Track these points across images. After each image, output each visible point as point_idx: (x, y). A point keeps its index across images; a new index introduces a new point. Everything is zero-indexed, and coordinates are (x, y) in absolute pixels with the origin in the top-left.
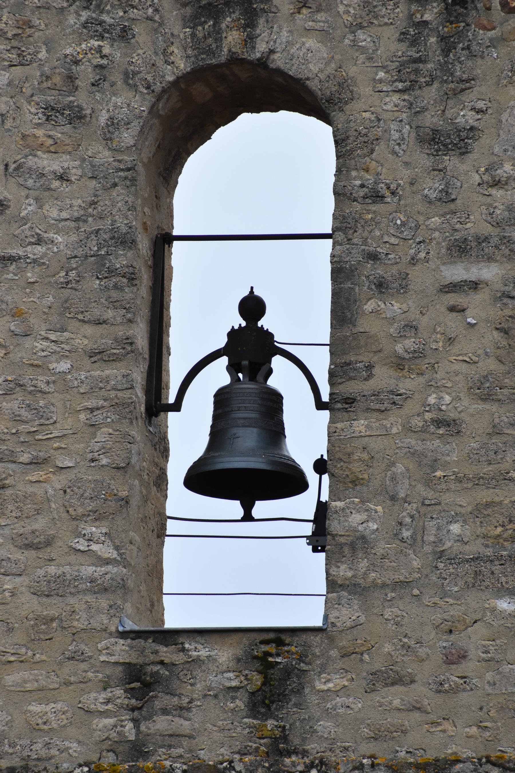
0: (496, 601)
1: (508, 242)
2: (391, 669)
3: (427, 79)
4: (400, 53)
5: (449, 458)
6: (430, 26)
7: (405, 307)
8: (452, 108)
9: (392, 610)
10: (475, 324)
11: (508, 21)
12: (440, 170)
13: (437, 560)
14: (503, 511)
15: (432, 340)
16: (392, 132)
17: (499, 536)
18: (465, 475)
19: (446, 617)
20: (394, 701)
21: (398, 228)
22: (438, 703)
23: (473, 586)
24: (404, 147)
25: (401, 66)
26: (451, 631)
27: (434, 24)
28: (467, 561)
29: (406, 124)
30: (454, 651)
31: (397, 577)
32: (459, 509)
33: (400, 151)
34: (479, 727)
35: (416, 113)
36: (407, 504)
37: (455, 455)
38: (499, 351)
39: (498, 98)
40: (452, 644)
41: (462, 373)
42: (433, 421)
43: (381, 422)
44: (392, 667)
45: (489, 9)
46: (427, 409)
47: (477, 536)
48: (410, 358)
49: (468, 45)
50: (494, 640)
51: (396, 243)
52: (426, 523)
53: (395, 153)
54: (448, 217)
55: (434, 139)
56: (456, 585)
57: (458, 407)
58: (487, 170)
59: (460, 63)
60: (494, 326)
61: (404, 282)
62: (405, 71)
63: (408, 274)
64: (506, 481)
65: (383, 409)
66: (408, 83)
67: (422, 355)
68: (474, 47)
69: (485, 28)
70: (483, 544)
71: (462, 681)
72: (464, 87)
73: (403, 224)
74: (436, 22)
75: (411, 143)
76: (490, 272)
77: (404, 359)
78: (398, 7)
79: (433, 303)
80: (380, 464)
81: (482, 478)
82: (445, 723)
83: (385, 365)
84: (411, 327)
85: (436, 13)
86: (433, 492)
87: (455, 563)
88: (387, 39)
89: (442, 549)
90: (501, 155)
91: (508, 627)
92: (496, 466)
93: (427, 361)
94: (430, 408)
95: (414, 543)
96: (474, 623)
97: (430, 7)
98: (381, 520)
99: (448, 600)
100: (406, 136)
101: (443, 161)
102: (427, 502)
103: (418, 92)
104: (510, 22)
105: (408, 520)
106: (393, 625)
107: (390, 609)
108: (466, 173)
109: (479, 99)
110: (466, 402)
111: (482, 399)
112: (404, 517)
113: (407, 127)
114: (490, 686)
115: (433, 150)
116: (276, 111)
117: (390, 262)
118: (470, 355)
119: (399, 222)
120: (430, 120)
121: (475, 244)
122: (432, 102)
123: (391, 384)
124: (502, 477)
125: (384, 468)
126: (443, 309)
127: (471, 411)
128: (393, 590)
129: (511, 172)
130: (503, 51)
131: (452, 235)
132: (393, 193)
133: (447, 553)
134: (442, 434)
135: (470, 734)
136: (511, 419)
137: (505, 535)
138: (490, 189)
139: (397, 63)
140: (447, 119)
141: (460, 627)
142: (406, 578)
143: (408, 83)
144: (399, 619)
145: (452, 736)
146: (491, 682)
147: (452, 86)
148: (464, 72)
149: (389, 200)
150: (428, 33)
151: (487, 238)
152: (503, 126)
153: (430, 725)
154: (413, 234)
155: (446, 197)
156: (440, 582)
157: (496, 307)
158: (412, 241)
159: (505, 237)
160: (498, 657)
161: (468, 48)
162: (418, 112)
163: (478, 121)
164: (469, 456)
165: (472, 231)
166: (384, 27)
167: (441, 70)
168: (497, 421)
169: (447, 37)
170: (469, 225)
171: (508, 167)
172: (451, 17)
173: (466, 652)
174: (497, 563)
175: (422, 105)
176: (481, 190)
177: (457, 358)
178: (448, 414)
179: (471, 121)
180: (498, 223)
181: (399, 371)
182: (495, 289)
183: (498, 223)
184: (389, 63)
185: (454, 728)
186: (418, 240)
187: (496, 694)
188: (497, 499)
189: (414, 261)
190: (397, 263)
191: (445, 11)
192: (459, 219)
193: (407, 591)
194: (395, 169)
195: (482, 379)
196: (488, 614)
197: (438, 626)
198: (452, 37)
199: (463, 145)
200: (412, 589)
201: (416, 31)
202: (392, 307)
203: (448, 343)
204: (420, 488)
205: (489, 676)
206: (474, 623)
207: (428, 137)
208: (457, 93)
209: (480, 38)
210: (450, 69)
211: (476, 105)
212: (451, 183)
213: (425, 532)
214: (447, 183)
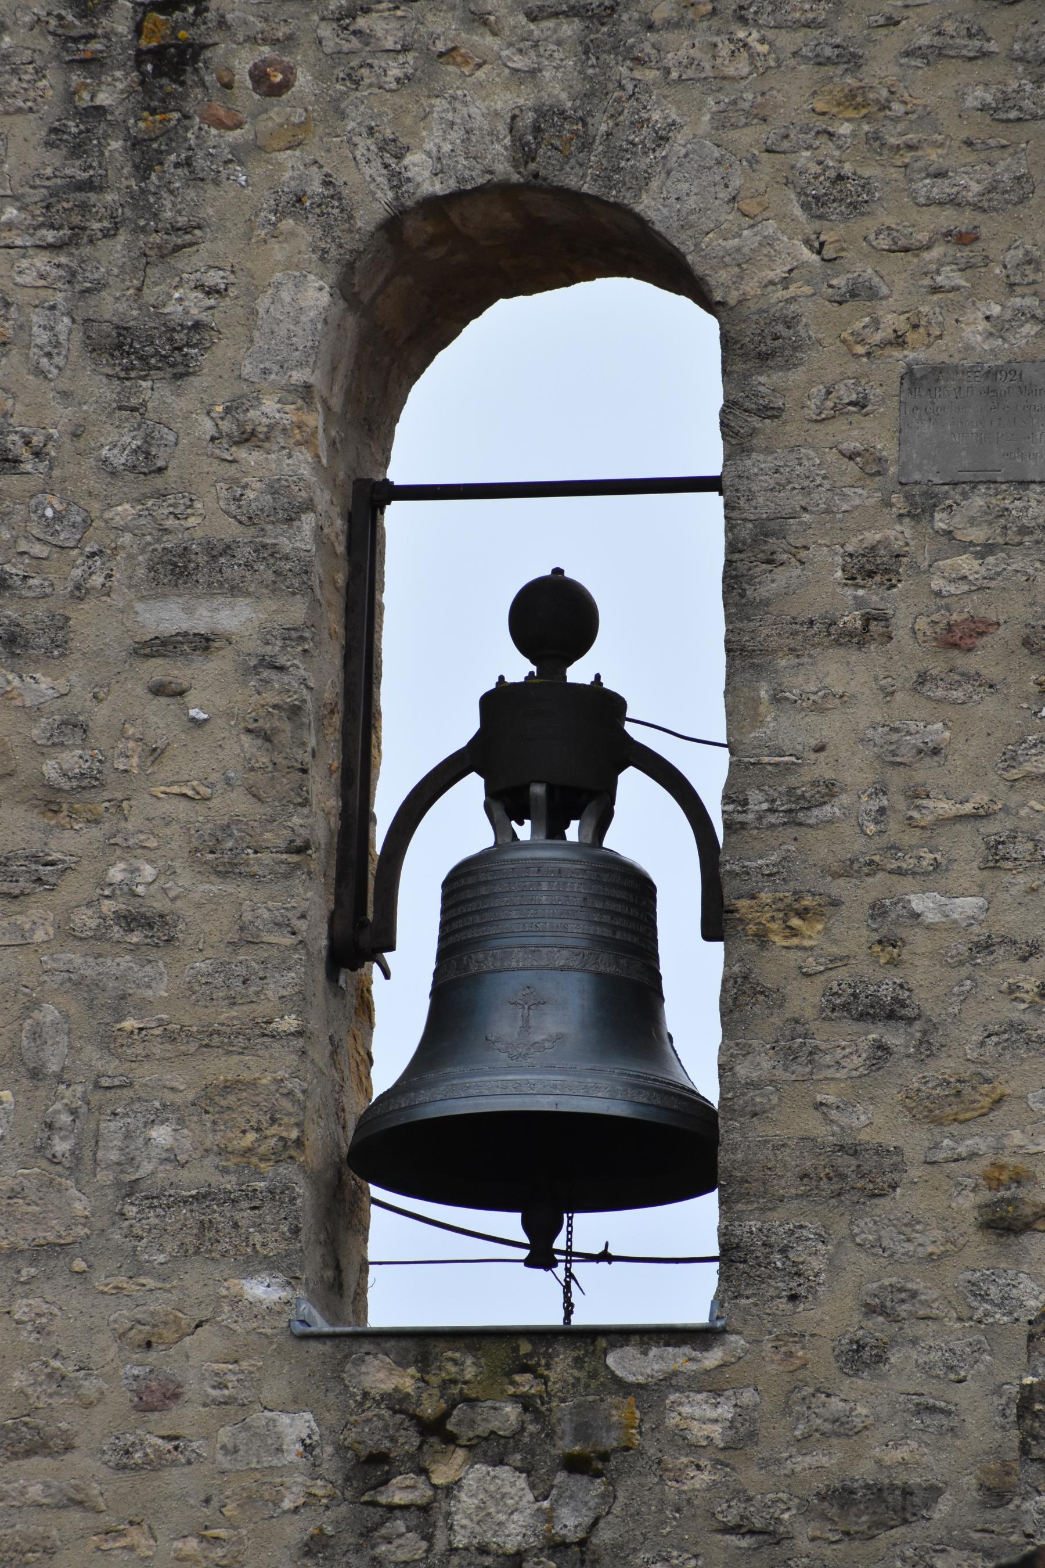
1: (272, 555)
2: (26, 1424)
3: (106, 224)
4: (49, 171)
5: (150, 992)
6: (109, 118)
7: (62, 686)
8: (156, 284)
10: (205, 720)
11: (266, 111)
12: (133, 409)
13: (123, 1199)
14: (258, 1099)
15: (117, 752)
16: (35, 329)
17: (250, 1150)
19: (139, 1316)
20: (31, 1489)
21: (48, 526)
23: (197, 1252)
24: (59, 360)
25: (51, 196)
28: (185, 1202)
29: (63, 314)
30: (154, 1385)
32: (169, 1097)
33: (52, 369)
34: (202, 1538)
35: (84, 291)
36: (63, 1087)
37: (163, 986)
38: (253, 777)
39: (249, 265)
40: (151, 1371)
41: (178, 821)
43: (12, 919)
44: (26, 1419)
45: (228, 86)
46: (106, 893)
47: (206, 1151)
48: (73, 789)
50: (236, 1362)
51: (44, 555)
52: (103, 1125)
53: (40, 372)
54: (150, 503)
55: (120, 346)
57: (170, 889)
58: (228, 410)
59: (171, 192)
60: (242, 725)
61: (61, 634)
62: (59, 207)
63: (68, 619)
64: (265, 1039)
65: (17, 892)
66: (67, 232)
67: (96, 783)
69: (220, 124)
70: (217, 1168)
71: (169, 1446)
72: (179, 241)
73: (59, 517)
74: (121, 109)
75: (74, 353)
76: (235, 617)
78: (44, 76)
79: (119, 678)
82: (133, 1531)
83: (22, 802)
84: (75, 726)
85: (122, 92)
86: (117, 1062)
89: (133, 1178)
91: (265, 1335)
92: (245, 1008)
94: (113, 891)
95: (77, 1165)
96: (197, 1326)
98: (11, 1119)
99: (143, 1281)
100: (62, 338)
102: (105, 1082)
103: (87, 251)
104: (272, 114)
105: (65, 1118)
106: (31, 1332)
107: (25, 1301)
108: (187, 416)
109: (210, 267)
110: (185, 878)
111: (218, 873)
112: (59, 1112)
113: (66, 320)
114: (226, 1455)
115: (118, 369)
116: (593, 279)
117: (31, 594)
118: (195, 783)
119: (49, 513)
120: (113, 306)
122: (116, 271)
123: (34, 842)
124: (258, 1032)
125: (16, 1014)
126: (140, 690)
127: (196, 897)
128: (33, 1262)
129: (277, 415)
131: (158, 541)
132: (37, 454)
133: (143, 1185)
134: (136, 944)
135: (183, 1554)
136: (277, 913)
137: (262, 1150)
138: (234, 449)
139: (44, 191)
140: (147, 305)
141: (169, 1335)
142: (60, 1237)
143: (67, 232)
144: (44, 1320)
145: (147, 1557)
146: (230, 1446)
147: (155, 238)
149: (28, 467)
150: (105, 131)
151: (228, 547)
152: (260, 322)
153: (102, 1536)
154: (78, 537)
155: (146, 464)
156: (129, 1244)
157: (247, 686)
158: (76, 551)
159: (264, 546)
160: (243, 1395)
161: (188, 163)
162: (88, 290)
164: (191, 989)
165: (199, 534)
167: (134, 206)
168: (248, 916)
169: (144, 140)
170: (192, 521)
171: (270, 405)
172: (151, 99)
173: (179, 1386)
174: (245, 1204)
175: (96, 276)
177: (168, 790)
178: (148, 902)
179: (194, 311)
180: (250, 518)
181: (50, 814)
182: (245, 650)
183: (250, 518)
184: (27, 189)
185: (152, 1542)
186: (88, 549)
187: (238, 1471)
188: (246, 1076)
189: (80, 592)
190: (46, 596)
191: (140, 88)
192: (171, 509)
193: (61, 1263)
195: (219, 833)
196: (226, 1309)
197: (124, 1334)
198: (155, 140)
199: (179, 359)
200: (72, 1260)
201: (82, 127)
202: (35, 686)
203: (151, 758)
204: (91, 1053)
205: (224, 1435)
206: (197, 1326)
208: (167, 253)
210: (151, 206)
212: (156, 434)
213: (100, 1144)
214: (147, 435)
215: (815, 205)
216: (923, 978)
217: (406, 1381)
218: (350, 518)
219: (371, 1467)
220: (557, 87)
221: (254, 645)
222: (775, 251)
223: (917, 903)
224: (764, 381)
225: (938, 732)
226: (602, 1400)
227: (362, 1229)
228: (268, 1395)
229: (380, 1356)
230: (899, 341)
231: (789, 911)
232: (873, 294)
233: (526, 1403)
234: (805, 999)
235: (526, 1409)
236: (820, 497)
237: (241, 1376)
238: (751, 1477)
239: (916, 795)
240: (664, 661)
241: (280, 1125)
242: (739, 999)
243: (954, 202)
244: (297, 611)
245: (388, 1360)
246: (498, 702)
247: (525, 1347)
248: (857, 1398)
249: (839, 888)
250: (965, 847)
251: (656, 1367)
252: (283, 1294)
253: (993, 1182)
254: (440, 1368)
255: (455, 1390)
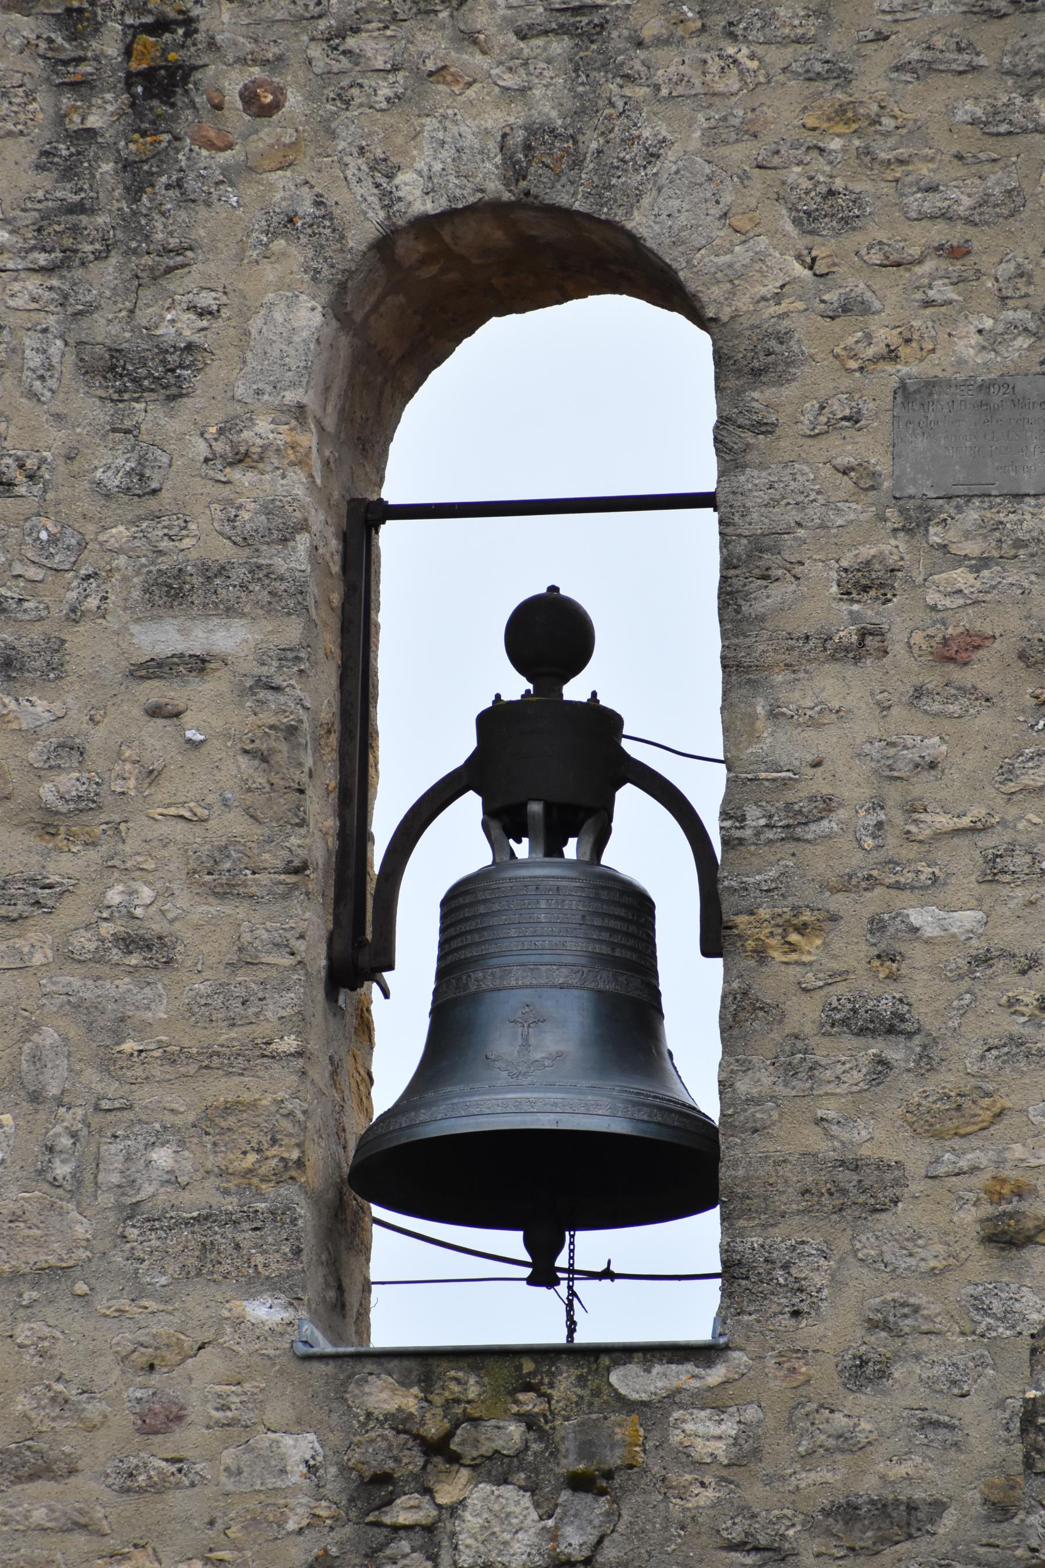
0: (245, 1303)
1: (267, 576)
2: (29, 1448)
4: (40, 194)
5: (150, 1014)
6: (100, 140)
7: (58, 708)
8: (148, 306)
9: (33, 1325)
11: (257, 132)
12: (127, 432)
14: (258, 1120)
16: (28, 352)
18: (182, 1048)
19: (142, 1339)
20: (35, 1513)
21: (43, 548)
22: (123, 1514)
23: (199, 1274)
24: (52, 383)
25: (42, 219)
26: (152, 1367)
27: (109, 136)
28: (186, 1224)
29: (55, 337)
30: (157, 1407)
31: (42, 1258)
32: (169, 1119)
37: (162, 1008)
38: (249, 798)
39: (241, 286)
40: (154, 1394)
41: (175, 842)
42: (117, 940)
45: (219, 107)
46: (105, 915)
47: (208, 1172)
48: (70, 812)
49: (179, 180)
51: (40, 577)
52: (104, 1148)
53: (33, 395)
54: (144, 525)
55: (112, 368)
56: (163, 1273)
58: (221, 431)
59: (163, 214)
61: (56, 656)
62: (50, 230)
63: (63, 642)
64: (265, 1060)
65: (15, 915)
68: (191, 184)
69: (211, 145)
70: (218, 1189)
71: (173, 1468)
72: (171, 263)
73: (53, 540)
74: (112, 131)
76: (230, 638)
77: (57, 813)
78: (34, 100)
79: (115, 700)
80: (8, 1028)
81: (218, 1054)
82: (137, 1553)
84: (71, 749)
85: (112, 114)
86: (117, 1084)
87: (162, 1228)
88: (13, 165)
90: (249, 401)
92: (244, 1029)
93: (104, 817)
94: (111, 914)
95: (78, 1188)
96: (200, 1348)
97: (100, 101)
98: (11, 1142)
99: (146, 1303)
100: (55, 360)
101: (133, 413)
102: (105, 1104)
103: (78, 273)
104: (262, 135)
105: (66, 1141)
107: (27, 1325)
110: (183, 900)
111: (216, 895)
112: (57, 1135)
113: (59, 343)
115: (111, 391)
117: (27, 617)
118: (192, 804)
119: (44, 535)
120: (105, 328)
121: (201, 580)
122: (108, 293)
124: (257, 1053)
125: (16, 1037)
126: (137, 712)
127: (194, 918)
128: (35, 1285)
129: (271, 436)
130: (249, 192)
131: (153, 563)
132: (31, 477)
133: (145, 1207)
134: (135, 966)
137: (263, 1171)
138: (228, 470)
139: (36, 214)
141: (171, 1357)
142: (62, 1260)
144: (46, 1344)
146: (233, 1468)
148: (171, 234)
149: (22, 490)
150: (96, 154)
152: (252, 343)
154: (73, 559)
155: (140, 486)
156: (130, 1266)
157: (243, 707)
158: (71, 573)
159: (259, 567)
160: (246, 1417)
161: (179, 184)
162: (80, 313)
163: (203, 333)
164: (190, 1010)
165: (194, 555)
166: (5, 140)
167: (126, 228)
168: (247, 937)
169: (135, 162)
170: (187, 543)
171: (263, 426)
172: (142, 121)
173: (182, 1408)
174: (246, 1226)
175: (88, 298)
176: (211, 472)
177: (165, 812)
178: (146, 924)
179: (187, 333)
181: (47, 837)
182: (242, 671)
186: (83, 572)
187: (241, 1493)
188: (247, 1097)
189: (75, 615)
192: (166, 531)
194: (34, 428)
195: (216, 854)
196: (229, 1330)
197: (126, 1357)
198: (146, 161)
199: (172, 381)
200: (74, 1283)
201: (73, 150)
202: (31, 709)
204: (91, 1076)
205: (228, 1457)
206: (200, 1348)
207: (101, 363)
209: (202, 165)
210: (142, 228)
211: (197, 299)
213: (101, 1166)
214: (141, 457)
215: (806, 221)
216: (923, 992)
217: (409, 1401)
218: (345, 538)
219: (376, 1487)
220: (547, 104)
221: (251, 667)
222: (766, 267)
223: (916, 917)
224: (758, 397)
225: (934, 746)
226: (605, 1418)
227: (364, 1249)
228: (271, 1416)
229: (383, 1376)
230: (891, 355)
231: (788, 926)
232: (866, 309)
233: (530, 1422)
234: (805, 1014)
235: (529, 1428)
236: (815, 512)
237: (244, 1398)
238: (755, 1493)
239: (913, 809)
240: (659, 677)
241: (281, 1146)
242: (738, 1015)
243: (945, 216)
244: (292, 631)
245: (390, 1380)
246: (495, 721)
247: (528, 1366)
248: (862, 1414)
249: (836, 903)
250: (963, 861)
251: (659, 1384)
252: (285, 1315)
253: (995, 1196)
254: (443, 1388)
255: (458, 1410)
